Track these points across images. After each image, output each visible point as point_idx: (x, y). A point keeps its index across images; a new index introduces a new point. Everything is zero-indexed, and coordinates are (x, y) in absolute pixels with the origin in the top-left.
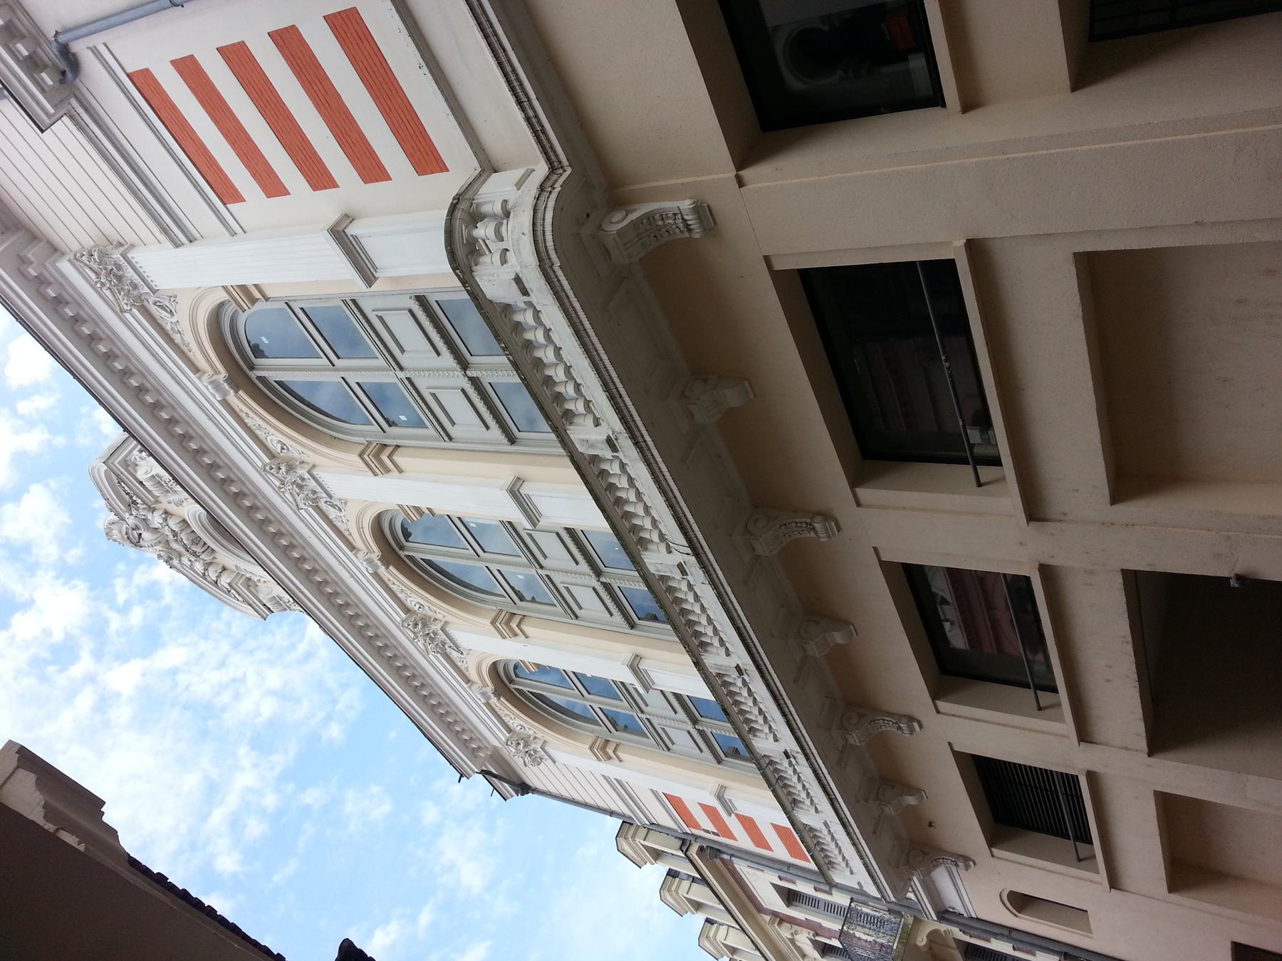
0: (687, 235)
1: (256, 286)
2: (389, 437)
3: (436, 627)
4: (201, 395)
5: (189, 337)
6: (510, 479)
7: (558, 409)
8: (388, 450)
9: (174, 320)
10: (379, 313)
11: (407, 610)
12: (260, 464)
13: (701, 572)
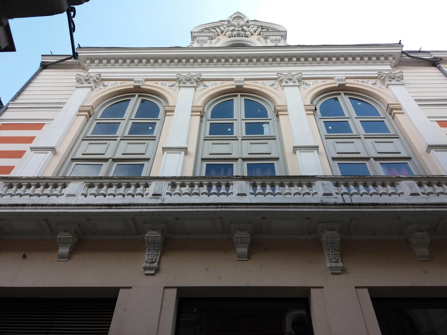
2: (93, 120)
3: (92, 85)
5: (159, 86)
6: (57, 150)
7: (361, 182)
8: (88, 116)
9: (167, 85)
10: (107, 144)
11: (103, 80)
12: (202, 74)
13: (128, 203)
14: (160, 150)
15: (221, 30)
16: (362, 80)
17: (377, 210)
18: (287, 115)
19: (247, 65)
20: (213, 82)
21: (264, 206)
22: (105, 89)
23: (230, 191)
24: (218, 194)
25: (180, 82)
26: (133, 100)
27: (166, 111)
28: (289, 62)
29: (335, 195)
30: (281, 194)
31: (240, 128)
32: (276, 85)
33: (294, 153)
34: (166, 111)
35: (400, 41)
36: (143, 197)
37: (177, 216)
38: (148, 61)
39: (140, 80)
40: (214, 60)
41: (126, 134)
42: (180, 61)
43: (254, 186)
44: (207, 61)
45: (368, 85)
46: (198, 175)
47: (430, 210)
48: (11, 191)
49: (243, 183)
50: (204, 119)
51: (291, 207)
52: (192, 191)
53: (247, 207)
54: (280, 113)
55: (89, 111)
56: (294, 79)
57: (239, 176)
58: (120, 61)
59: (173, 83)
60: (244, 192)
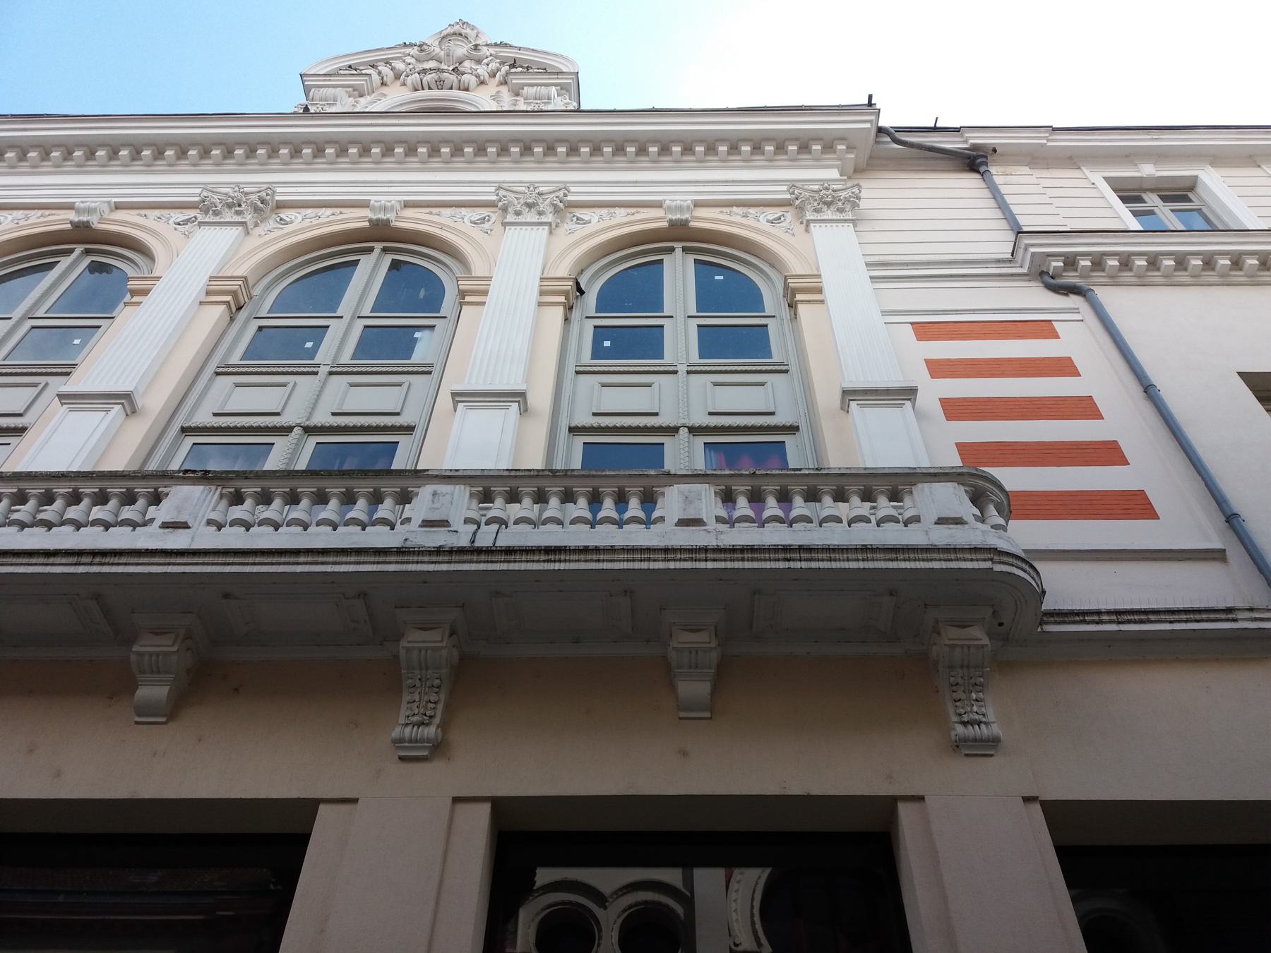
0: (402, 720)
1: (484, 303)
3: (248, 217)
4: (92, 193)
6: (139, 402)
8: (234, 309)
11: (281, 206)
12: (572, 189)
14: (444, 400)
15: (393, 69)
16: (745, 210)
17: (557, 566)
18: (822, 302)
19: (424, 166)
20: (309, 211)
21: (221, 560)
22: (281, 232)
23: (655, 515)
24: (620, 524)
25: (500, 208)
26: (366, 262)
27: (463, 294)
28: (594, 159)
29: (712, 525)
30: (808, 520)
31: (681, 340)
32: (788, 220)
33: (845, 408)
34: (463, 294)
35: (870, 97)
36: (392, 528)
37: (228, 588)
38: (136, 155)
39: (93, 205)
40: (605, 149)
41: (346, 358)
42: (365, 151)
43: (728, 498)
44: (515, 150)
45: (753, 226)
46: (559, 465)
47: (710, 565)
48: (238, 512)
49: (197, 491)
50: (576, 315)
51: (302, 559)
52: (541, 512)
53: (168, 560)
54: (799, 297)
55: (234, 294)
56: (544, 205)
57: (194, 472)
58: (353, 151)
59: (484, 212)
60: (182, 519)
